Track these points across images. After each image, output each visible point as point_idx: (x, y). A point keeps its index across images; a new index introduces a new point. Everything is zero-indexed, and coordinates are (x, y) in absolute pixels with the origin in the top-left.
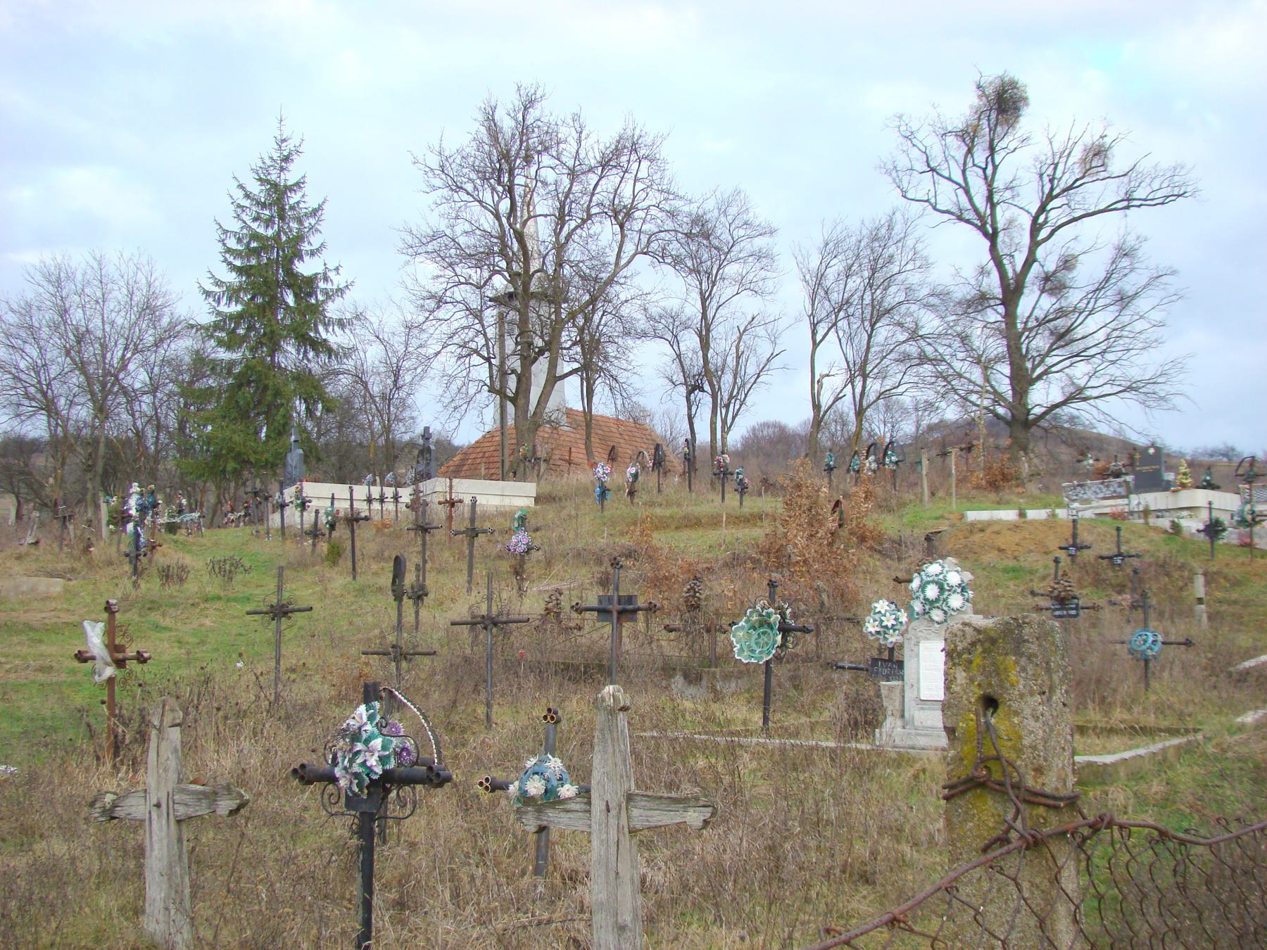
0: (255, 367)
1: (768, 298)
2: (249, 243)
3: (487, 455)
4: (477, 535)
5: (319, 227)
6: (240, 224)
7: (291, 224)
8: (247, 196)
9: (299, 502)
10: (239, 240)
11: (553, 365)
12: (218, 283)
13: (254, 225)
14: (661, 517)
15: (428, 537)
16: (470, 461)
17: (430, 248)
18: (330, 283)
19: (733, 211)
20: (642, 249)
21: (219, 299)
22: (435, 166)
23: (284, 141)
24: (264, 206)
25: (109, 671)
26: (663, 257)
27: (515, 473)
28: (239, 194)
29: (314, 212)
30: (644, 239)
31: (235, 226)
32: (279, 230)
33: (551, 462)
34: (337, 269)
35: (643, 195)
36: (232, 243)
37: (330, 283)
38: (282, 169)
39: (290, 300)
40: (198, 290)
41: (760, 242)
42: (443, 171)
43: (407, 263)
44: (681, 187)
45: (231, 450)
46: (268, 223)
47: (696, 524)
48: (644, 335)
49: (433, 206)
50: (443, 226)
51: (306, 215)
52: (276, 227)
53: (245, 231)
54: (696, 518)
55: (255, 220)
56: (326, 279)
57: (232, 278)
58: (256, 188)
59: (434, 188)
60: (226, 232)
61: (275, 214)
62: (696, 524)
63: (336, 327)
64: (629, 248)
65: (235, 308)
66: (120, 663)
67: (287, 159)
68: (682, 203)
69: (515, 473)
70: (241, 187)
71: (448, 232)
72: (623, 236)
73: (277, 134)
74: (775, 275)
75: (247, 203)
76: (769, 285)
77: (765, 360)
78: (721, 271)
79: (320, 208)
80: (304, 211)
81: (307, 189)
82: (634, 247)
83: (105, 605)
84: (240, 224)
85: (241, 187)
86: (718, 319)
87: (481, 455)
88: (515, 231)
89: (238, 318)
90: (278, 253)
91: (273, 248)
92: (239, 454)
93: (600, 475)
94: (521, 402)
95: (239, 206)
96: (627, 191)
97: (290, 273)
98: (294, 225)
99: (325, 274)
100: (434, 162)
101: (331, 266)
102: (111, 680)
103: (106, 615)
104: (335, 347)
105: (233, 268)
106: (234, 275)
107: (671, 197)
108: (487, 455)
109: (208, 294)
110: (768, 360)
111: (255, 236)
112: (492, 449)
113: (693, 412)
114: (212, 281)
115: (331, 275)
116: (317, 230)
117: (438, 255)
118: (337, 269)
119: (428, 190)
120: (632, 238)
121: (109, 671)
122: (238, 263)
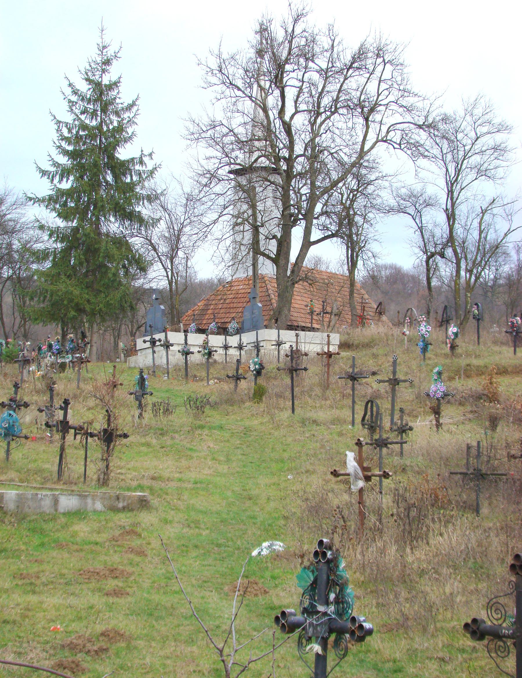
0: (89, 234)
1: (499, 181)
2: (78, 132)
3: (227, 301)
4: (398, 384)
5: (135, 120)
6: (73, 117)
7: (111, 117)
8: (75, 92)
9: (206, 351)
10: (70, 131)
11: (307, 232)
12: (56, 164)
13: (83, 117)
14: (478, 366)
15: (357, 386)
16: (212, 307)
17: (208, 135)
18: (144, 167)
19: (478, 112)
20: (382, 138)
21: (53, 177)
22: (215, 66)
23: (104, 47)
24: (89, 101)
25: (361, 484)
26: (400, 144)
27: (277, 321)
28: (68, 91)
29: (130, 107)
30: (384, 129)
31: (69, 118)
32: (102, 122)
33: (342, 315)
34: (150, 155)
35: (386, 93)
36: (66, 133)
37: (144, 167)
38: (104, 71)
39: (110, 178)
40: (35, 169)
41: (499, 138)
42: (221, 71)
43: (189, 146)
44: (414, 86)
45: (71, 301)
46: (94, 114)
47: (504, 372)
48: (391, 210)
49: (214, 101)
50: (220, 116)
51: (123, 109)
52: (99, 119)
53: (77, 123)
54: (504, 367)
55: (83, 113)
56: (141, 162)
57: (63, 160)
58: (84, 87)
59: (211, 85)
60: (59, 122)
61: (99, 108)
62: (504, 372)
63: (145, 201)
64: (372, 137)
65: (66, 185)
66: (367, 479)
67: (107, 62)
68: (416, 99)
69: (277, 321)
70: (70, 85)
71: (225, 122)
72: (368, 127)
73: (99, 41)
74: (508, 164)
75: (74, 98)
76: (500, 172)
77: (502, 235)
78: (465, 161)
79: (133, 104)
80: (120, 106)
81: (122, 87)
82: (376, 136)
83: (356, 441)
84: (73, 117)
85: (70, 85)
86: (462, 197)
87: (222, 301)
88: (284, 123)
89: (68, 193)
90: (100, 140)
91: (97, 136)
92: (77, 304)
93: (423, 332)
94: (282, 262)
95: (70, 101)
96: (372, 88)
97: (111, 157)
98: (114, 118)
99: (141, 158)
100: (214, 64)
101: (146, 152)
102: (361, 491)
103: (356, 448)
104: (146, 217)
105: (65, 153)
106: (66, 158)
107: (406, 94)
108: (227, 301)
109: (44, 173)
110: (506, 235)
111: (84, 127)
112: (231, 296)
113: (431, 275)
114: (51, 163)
115: (146, 159)
116: (134, 123)
117: (215, 142)
118: (150, 155)
119: (205, 86)
120: (374, 128)
121: (361, 484)
122: (70, 148)
